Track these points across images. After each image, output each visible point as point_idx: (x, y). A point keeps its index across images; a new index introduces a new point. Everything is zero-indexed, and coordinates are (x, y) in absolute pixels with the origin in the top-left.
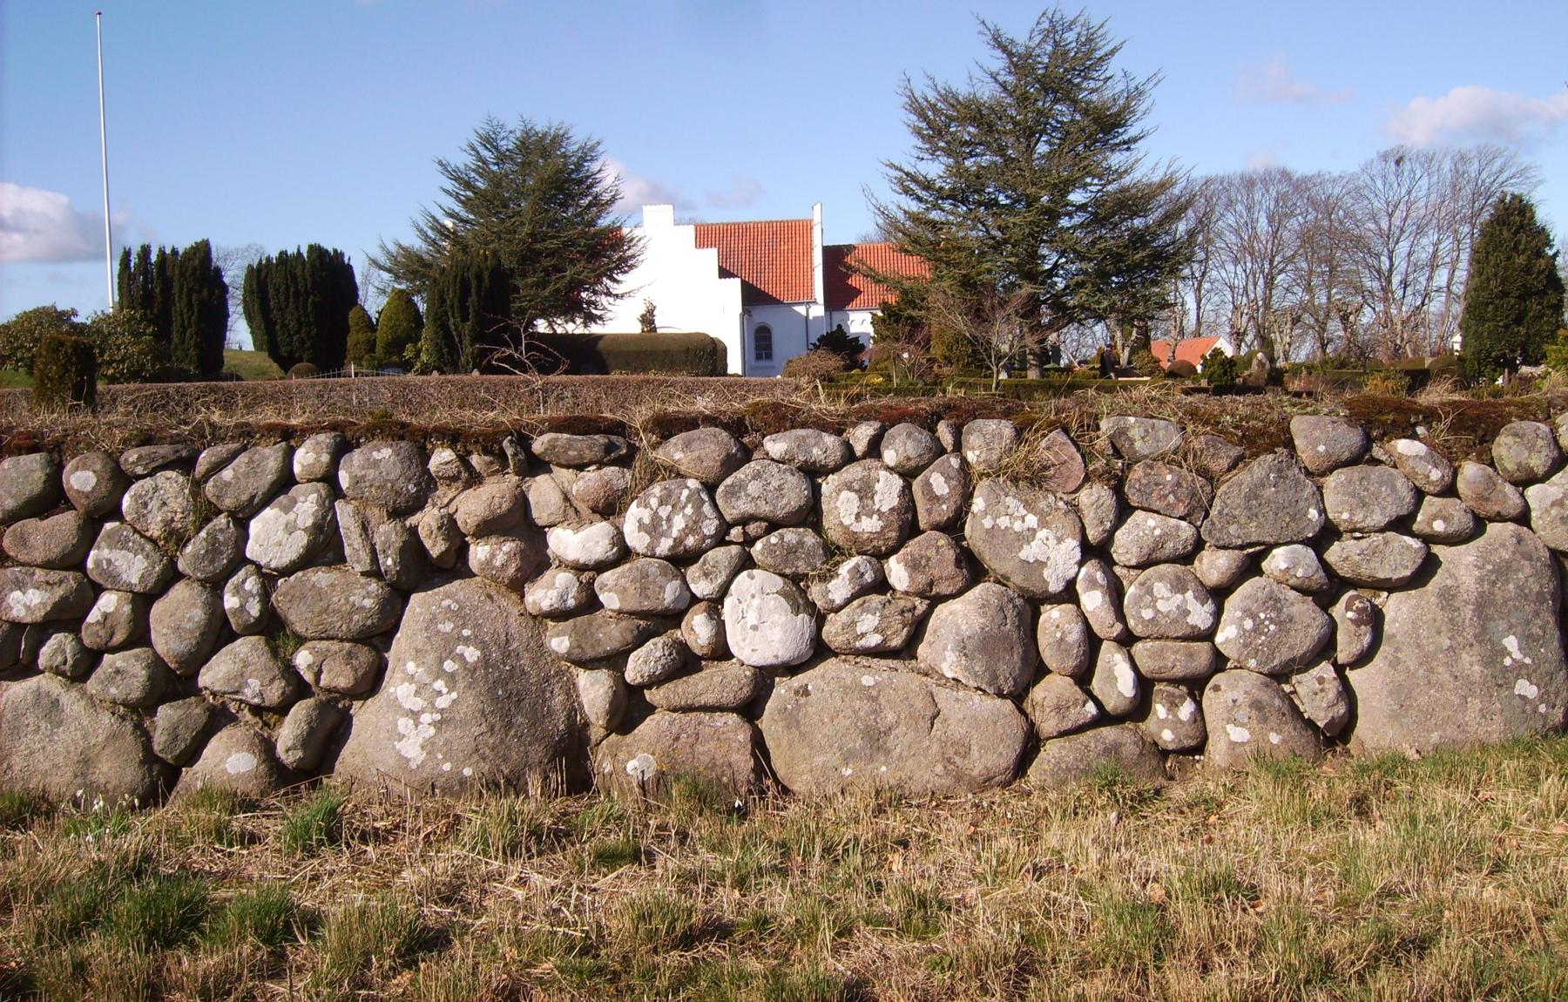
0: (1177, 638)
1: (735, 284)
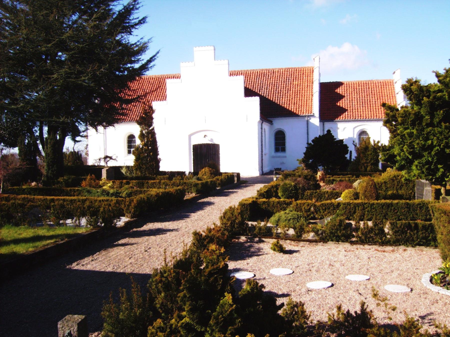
0: (172, 230)
1: (256, 100)
